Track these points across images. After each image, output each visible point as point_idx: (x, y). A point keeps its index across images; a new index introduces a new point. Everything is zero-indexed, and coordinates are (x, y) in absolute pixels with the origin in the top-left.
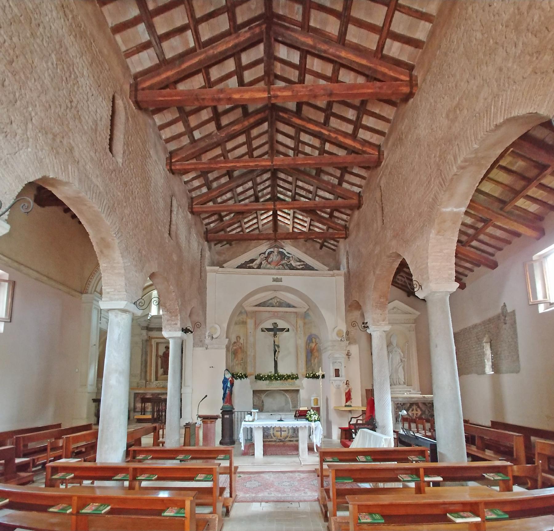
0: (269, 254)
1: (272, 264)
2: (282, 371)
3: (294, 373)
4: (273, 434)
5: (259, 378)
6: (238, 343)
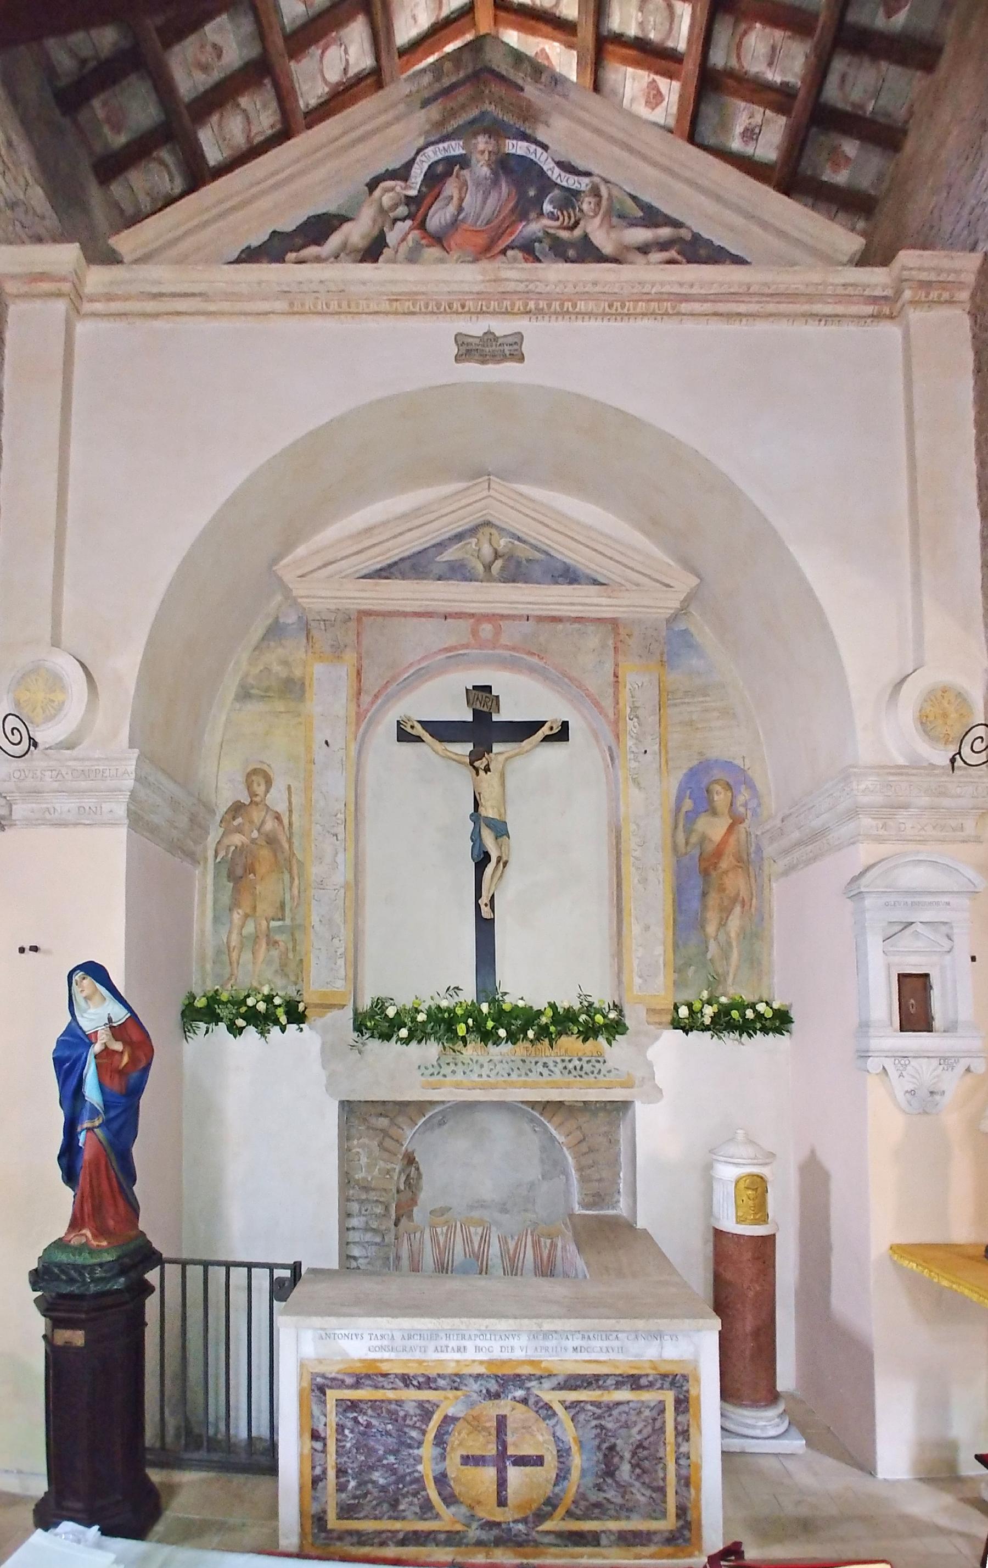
0: (435, 178)
2: (521, 985)
3: (601, 996)
4: (441, 1479)
5: (377, 1024)
6: (257, 815)
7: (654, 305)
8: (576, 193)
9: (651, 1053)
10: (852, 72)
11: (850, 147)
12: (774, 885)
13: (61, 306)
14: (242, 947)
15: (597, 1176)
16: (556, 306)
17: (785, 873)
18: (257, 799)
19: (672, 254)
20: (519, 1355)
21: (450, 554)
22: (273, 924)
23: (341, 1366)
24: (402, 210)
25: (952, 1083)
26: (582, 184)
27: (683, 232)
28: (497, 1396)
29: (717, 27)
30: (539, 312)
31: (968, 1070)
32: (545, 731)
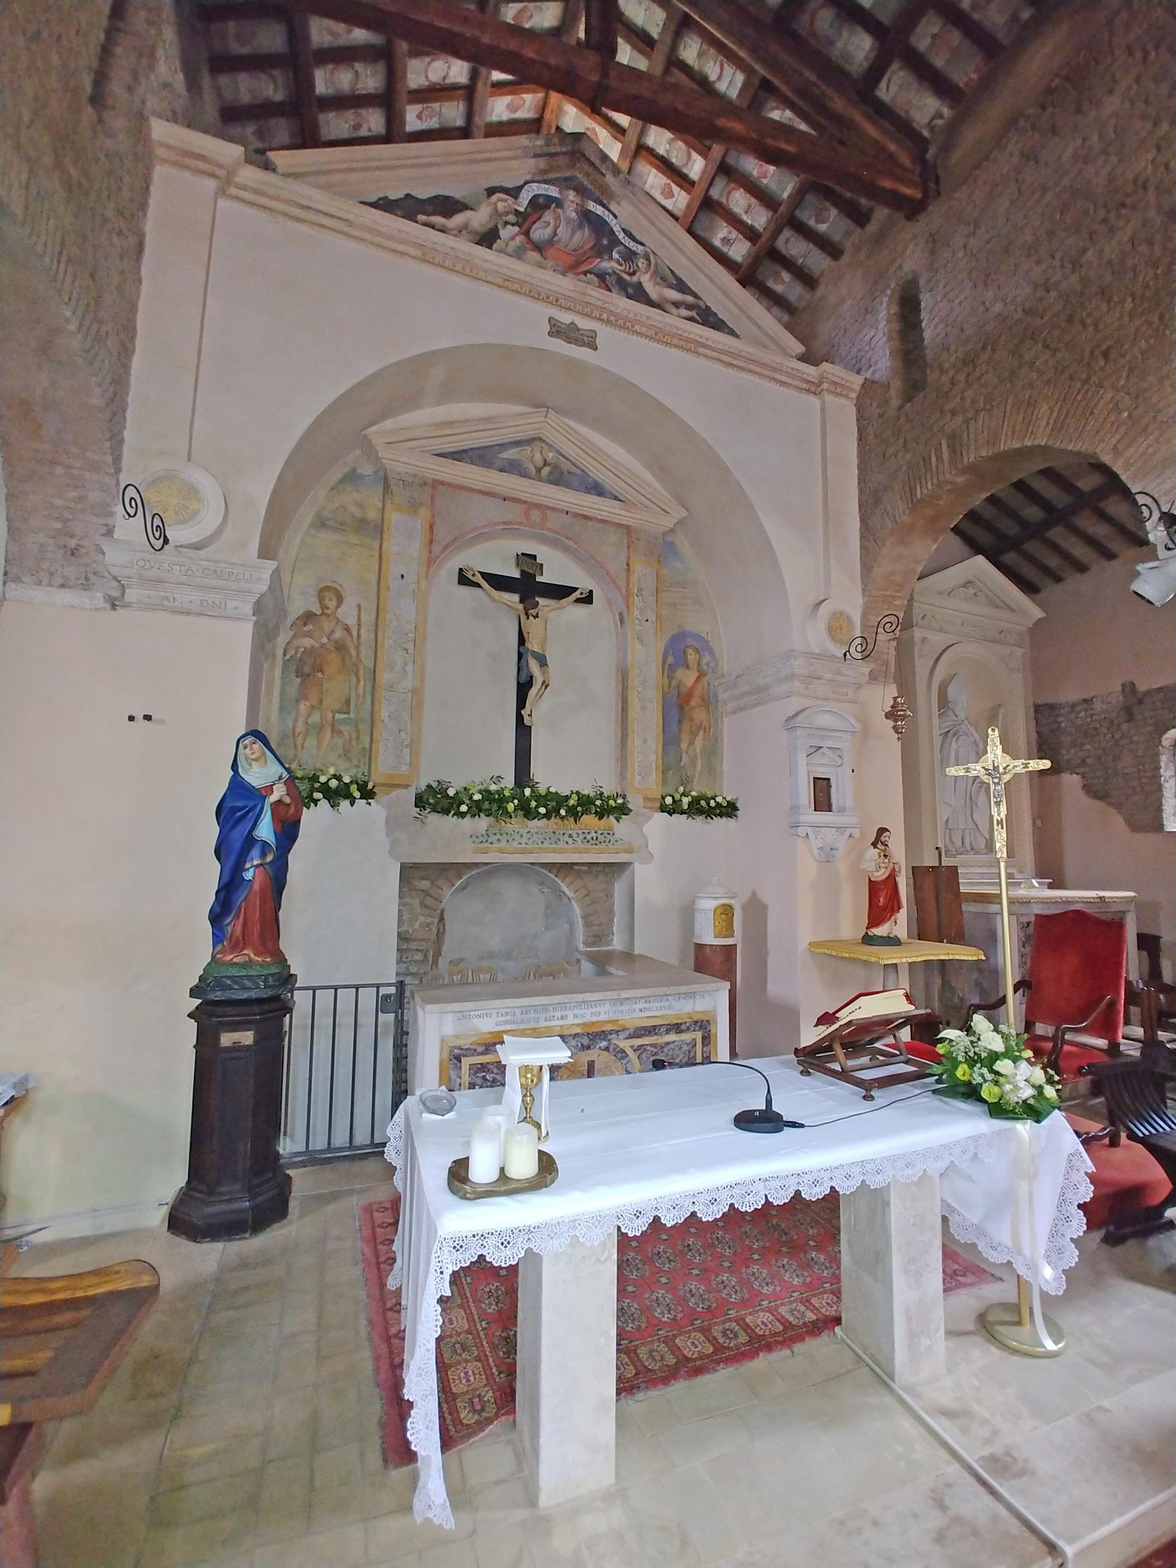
0: (539, 205)
1: (551, 252)
2: (552, 774)
5: (436, 801)
6: (327, 625)
7: (682, 343)
8: (635, 254)
9: (646, 829)
10: (793, 239)
11: (786, 276)
12: (725, 720)
13: (211, 184)
14: (307, 733)
15: (597, 922)
16: (621, 322)
17: (734, 712)
18: (329, 611)
19: (693, 314)
20: (603, 1017)
21: (510, 454)
22: (338, 716)
23: (474, 1039)
24: (511, 218)
25: (842, 843)
26: (639, 249)
27: (701, 303)
28: (589, 1048)
29: (717, 179)
30: (608, 322)
31: (850, 836)
32: (577, 595)
